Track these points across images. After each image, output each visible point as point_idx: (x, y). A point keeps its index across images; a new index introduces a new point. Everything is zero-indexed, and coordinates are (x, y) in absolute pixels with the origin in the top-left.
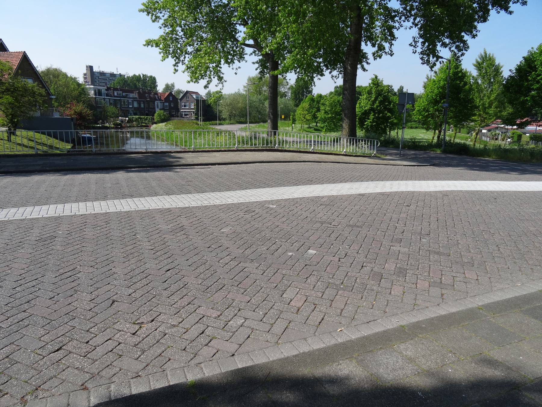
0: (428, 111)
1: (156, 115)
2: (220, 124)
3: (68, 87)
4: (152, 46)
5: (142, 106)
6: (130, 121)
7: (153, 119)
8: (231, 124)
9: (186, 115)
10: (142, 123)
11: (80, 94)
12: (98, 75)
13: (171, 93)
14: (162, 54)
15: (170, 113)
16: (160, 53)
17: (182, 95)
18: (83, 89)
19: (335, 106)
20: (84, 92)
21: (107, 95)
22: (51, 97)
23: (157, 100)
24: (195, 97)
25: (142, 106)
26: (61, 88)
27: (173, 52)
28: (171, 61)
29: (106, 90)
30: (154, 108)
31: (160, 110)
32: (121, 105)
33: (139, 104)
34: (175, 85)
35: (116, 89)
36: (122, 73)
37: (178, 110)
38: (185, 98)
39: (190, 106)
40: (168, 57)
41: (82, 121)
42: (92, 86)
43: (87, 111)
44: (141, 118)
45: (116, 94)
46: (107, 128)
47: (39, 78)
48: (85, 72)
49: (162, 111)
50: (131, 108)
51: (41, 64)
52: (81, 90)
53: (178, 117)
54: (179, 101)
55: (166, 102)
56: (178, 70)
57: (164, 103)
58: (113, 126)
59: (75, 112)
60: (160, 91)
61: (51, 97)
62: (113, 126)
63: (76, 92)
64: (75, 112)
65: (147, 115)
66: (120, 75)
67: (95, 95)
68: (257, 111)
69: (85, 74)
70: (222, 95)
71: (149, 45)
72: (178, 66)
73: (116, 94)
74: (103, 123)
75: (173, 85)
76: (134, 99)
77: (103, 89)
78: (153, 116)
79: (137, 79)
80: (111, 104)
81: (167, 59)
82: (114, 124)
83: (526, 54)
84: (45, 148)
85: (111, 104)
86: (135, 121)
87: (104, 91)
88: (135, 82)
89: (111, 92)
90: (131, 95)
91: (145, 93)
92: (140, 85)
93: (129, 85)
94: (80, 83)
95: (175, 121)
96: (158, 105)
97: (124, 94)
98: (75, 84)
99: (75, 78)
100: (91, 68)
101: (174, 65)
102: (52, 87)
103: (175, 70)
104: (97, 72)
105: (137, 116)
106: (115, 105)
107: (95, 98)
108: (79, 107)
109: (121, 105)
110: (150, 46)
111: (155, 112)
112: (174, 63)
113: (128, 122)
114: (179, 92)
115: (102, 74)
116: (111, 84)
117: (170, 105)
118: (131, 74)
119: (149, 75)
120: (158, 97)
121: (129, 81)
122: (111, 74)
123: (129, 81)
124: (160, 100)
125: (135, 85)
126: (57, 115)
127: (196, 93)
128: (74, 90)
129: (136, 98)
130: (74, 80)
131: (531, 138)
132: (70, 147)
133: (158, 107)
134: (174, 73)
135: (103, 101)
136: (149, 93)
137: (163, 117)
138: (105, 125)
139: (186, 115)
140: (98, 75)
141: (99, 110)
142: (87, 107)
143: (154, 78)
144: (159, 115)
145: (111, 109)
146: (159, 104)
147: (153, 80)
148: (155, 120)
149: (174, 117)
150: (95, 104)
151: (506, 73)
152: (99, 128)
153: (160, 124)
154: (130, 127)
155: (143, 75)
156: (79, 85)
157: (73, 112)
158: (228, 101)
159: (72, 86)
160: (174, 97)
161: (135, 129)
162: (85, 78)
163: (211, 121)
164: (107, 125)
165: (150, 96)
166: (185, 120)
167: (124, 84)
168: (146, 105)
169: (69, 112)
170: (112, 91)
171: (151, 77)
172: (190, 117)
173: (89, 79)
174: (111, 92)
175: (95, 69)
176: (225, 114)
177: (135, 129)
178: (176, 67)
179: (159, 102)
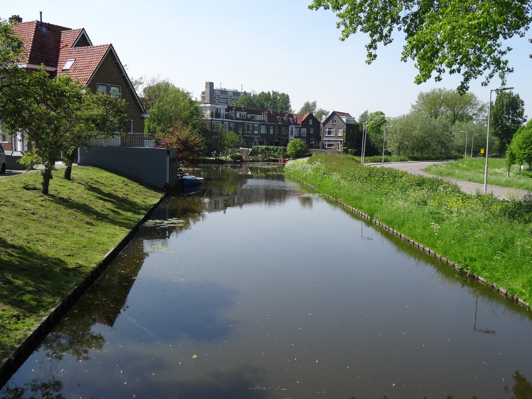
1: (289, 144)
2: (386, 161)
3: (177, 105)
4: (327, 8)
5: (272, 132)
6: (254, 153)
7: (285, 150)
8: (401, 161)
9: (330, 145)
10: (269, 155)
11: (192, 114)
12: (219, 93)
13: (311, 115)
14: (343, 27)
15: (308, 142)
16: (338, 26)
17: (324, 118)
18: (196, 108)
19: (39, 128)
20: (198, 112)
21: (227, 117)
22: (143, 115)
23: (291, 124)
24: (344, 120)
25: (272, 132)
26: (167, 107)
27: (368, 19)
28: (362, 38)
29: (227, 110)
30: (287, 135)
31: (296, 137)
32: (244, 130)
33: (268, 130)
34: (317, 104)
35: (239, 109)
36: (248, 91)
37: (318, 138)
38: (331, 121)
39: (337, 133)
40: (355, 30)
41: (187, 152)
42: (209, 105)
43: (196, 138)
44: (268, 149)
45: (238, 116)
46: (222, 162)
47: (129, 86)
48: (204, 90)
49: (299, 140)
51: (142, 71)
52: (194, 110)
53: (318, 147)
54: (322, 125)
55: (303, 126)
56: (375, 56)
57: (300, 128)
58: (230, 159)
59: (179, 139)
60: (296, 113)
61: (143, 115)
62: (230, 159)
63: (186, 113)
64: (179, 139)
65: (277, 144)
66: (245, 93)
67: (212, 116)
68: (439, 142)
69: (203, 93)
70: (384, 118)
71: (320, 5)
72: (375, 48)
73: (238, 116)
74: (217, 155)
75: (314, 104)
76: (262, 122)
77: (222, 109)
78: (286, 146)
79: (266, 97)
80: (230, 129)
81: (352, 36)
82: (232, 157)
83: (521, 98)
84: (109, 205)
85: (230, 129)
86: (261, 153)
87: (223, 112)
88: (263, 101)
89: (232, 113)
90: (259, 117)
91: (276, 114)
92: (267, 104)
93: (255, 105)
94: (193, 99)
95: (315, 153)
96: (292, 131)
97: (249, 116)
98: (186, 101)
99: (188, 93)
100: (211, 85)
101: (370, 46)
102: (156, 104)
103: (370, 55)
104: (218, 90)
105: (264, 147)
106: (236, 130)
107: (211, 120)
108: (185, 133)
110: (322, 8)
111: (288, 142)
112: (369, 41)
113: (251, 154)
114: (322, 113)
115: (224, 92)
116: (234, 104)
117: (308, 131)
118: (258, 92)
119: (280, 93)
120: (293, 121)
121: (255, 101)
122: (233, 92)
123: (255, 101)
124: (296, 124)
125: (262, 106)
126: (149, 145)
127: (347, 115)
128: (184, 109)
129: (264, 121)
130: (186, 95)
132: (156, 201)
133: (292, 134)
134: (369, 63)
135: (221, 124)
136: (282, 115)
137: (299, 148)
138: (220, 158)
139: (330, 145)
140: (219, 93)
141: (214, 137)
142: (199, 133)
143: (287, 97)
144: (294, 145)
145: (231, 136)
146: (294, 129)
147: (285, 99)
148: (288, 153)
149: (312, 148)
150: (209, 130)
152: (212, 162)
153: (300, 160)
154: (253, 161)
155: (274, 93)
156: (192, 103)
157: (175, 140)
158: (398, 126)
159: (183, 104)
160: (315, 120)
161: (259, 165)
162: (203, 98)
163: (373, 155)
164: (223, 158)
165: (282, 120)
166: (329, 153)
167: (249, 104)
169: (170, 140)
170: (234, 111)
171: (283, 95)
172: (335, 149)
173: (207, 100)
174: (232, 113)
175: (216, 87)
176: (392, 147)
177: (259, 165)
178: (372, 50)
179: (294, 126)
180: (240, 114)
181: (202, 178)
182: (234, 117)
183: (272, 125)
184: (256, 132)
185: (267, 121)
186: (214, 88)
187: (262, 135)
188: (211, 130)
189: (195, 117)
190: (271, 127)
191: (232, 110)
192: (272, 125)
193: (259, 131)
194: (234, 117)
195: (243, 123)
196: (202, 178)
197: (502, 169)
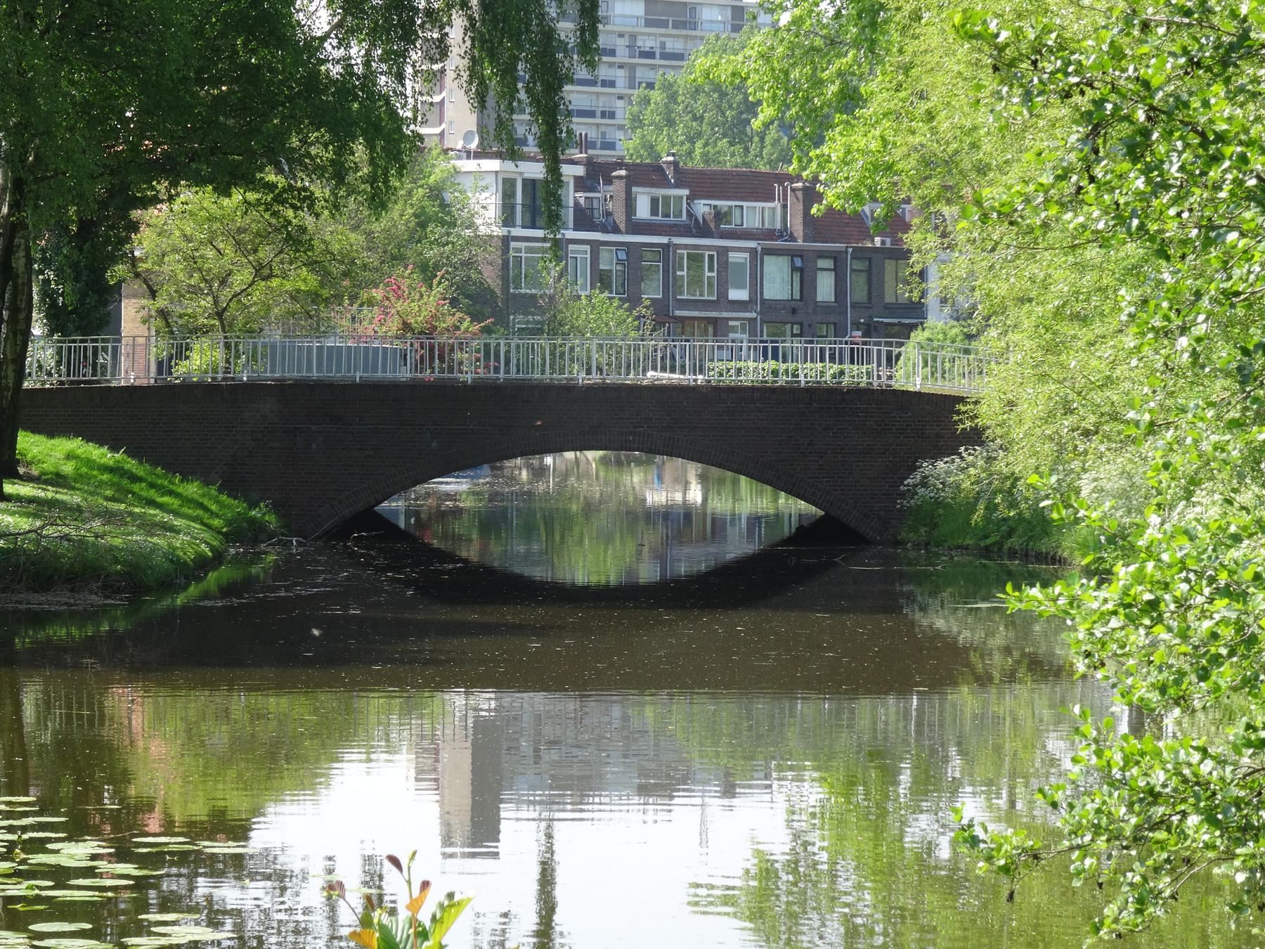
0: (1214, 847)
5: (825, 288)
20: (444, 206)
25: (825, 288)
32: (670, 283)
33: (804, 275)
42: (493, 165)
45: (643, 210)
50: (740, 305)
59: (406, 326)
64: (406, 326)
73: (643, 210)
89: (610, 195)
90: (754, 214)
97: (702, 208)
107: (506, 240)
108: (425, 305)
109: (670, 283)
129: (785, 233)
131: (223, 924)
151: (762, 820)
157: (394, 325)
168: (857, 290)
170: (617, 188)
180: (654, 202)
181: (63, 819)
182: (620, 218)
183: (822, 255)
184: (738, 294)
185: (798, 230)
186: (819, 299)
187: (769, 307)
188: (505, 288)
189: (435, 231)
190: (822, 263)
191: (609, 181)
192: (822, 255)
193: (756, 283)
194: (620, 218)
195: (666, 247)
196: (63, 819)
197: (237, 196)
